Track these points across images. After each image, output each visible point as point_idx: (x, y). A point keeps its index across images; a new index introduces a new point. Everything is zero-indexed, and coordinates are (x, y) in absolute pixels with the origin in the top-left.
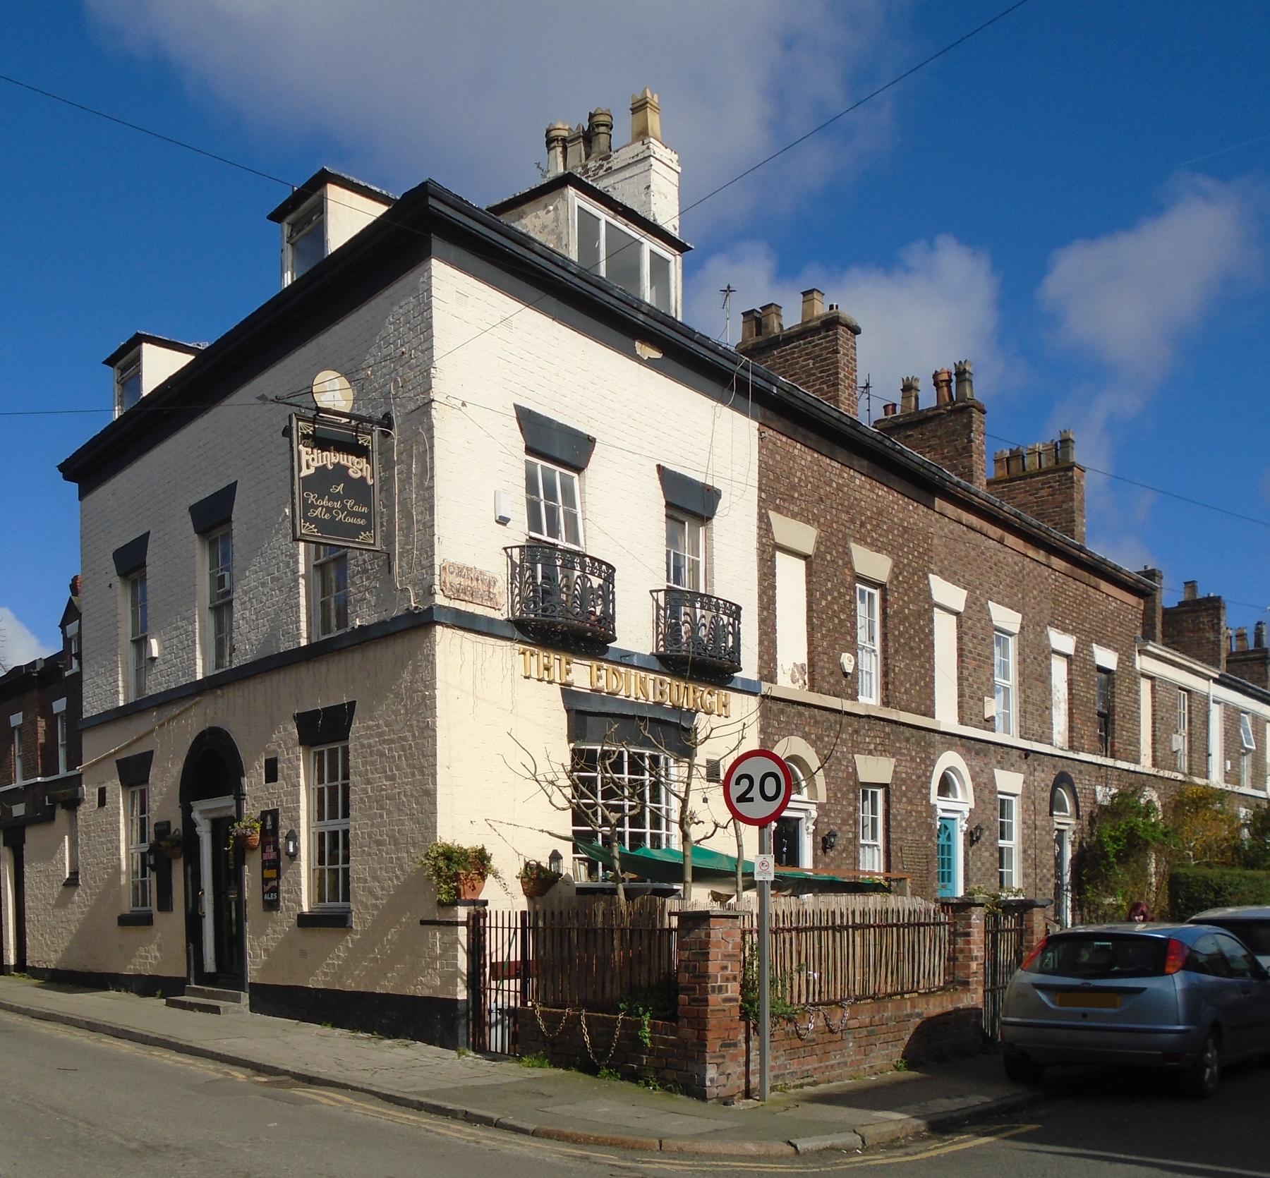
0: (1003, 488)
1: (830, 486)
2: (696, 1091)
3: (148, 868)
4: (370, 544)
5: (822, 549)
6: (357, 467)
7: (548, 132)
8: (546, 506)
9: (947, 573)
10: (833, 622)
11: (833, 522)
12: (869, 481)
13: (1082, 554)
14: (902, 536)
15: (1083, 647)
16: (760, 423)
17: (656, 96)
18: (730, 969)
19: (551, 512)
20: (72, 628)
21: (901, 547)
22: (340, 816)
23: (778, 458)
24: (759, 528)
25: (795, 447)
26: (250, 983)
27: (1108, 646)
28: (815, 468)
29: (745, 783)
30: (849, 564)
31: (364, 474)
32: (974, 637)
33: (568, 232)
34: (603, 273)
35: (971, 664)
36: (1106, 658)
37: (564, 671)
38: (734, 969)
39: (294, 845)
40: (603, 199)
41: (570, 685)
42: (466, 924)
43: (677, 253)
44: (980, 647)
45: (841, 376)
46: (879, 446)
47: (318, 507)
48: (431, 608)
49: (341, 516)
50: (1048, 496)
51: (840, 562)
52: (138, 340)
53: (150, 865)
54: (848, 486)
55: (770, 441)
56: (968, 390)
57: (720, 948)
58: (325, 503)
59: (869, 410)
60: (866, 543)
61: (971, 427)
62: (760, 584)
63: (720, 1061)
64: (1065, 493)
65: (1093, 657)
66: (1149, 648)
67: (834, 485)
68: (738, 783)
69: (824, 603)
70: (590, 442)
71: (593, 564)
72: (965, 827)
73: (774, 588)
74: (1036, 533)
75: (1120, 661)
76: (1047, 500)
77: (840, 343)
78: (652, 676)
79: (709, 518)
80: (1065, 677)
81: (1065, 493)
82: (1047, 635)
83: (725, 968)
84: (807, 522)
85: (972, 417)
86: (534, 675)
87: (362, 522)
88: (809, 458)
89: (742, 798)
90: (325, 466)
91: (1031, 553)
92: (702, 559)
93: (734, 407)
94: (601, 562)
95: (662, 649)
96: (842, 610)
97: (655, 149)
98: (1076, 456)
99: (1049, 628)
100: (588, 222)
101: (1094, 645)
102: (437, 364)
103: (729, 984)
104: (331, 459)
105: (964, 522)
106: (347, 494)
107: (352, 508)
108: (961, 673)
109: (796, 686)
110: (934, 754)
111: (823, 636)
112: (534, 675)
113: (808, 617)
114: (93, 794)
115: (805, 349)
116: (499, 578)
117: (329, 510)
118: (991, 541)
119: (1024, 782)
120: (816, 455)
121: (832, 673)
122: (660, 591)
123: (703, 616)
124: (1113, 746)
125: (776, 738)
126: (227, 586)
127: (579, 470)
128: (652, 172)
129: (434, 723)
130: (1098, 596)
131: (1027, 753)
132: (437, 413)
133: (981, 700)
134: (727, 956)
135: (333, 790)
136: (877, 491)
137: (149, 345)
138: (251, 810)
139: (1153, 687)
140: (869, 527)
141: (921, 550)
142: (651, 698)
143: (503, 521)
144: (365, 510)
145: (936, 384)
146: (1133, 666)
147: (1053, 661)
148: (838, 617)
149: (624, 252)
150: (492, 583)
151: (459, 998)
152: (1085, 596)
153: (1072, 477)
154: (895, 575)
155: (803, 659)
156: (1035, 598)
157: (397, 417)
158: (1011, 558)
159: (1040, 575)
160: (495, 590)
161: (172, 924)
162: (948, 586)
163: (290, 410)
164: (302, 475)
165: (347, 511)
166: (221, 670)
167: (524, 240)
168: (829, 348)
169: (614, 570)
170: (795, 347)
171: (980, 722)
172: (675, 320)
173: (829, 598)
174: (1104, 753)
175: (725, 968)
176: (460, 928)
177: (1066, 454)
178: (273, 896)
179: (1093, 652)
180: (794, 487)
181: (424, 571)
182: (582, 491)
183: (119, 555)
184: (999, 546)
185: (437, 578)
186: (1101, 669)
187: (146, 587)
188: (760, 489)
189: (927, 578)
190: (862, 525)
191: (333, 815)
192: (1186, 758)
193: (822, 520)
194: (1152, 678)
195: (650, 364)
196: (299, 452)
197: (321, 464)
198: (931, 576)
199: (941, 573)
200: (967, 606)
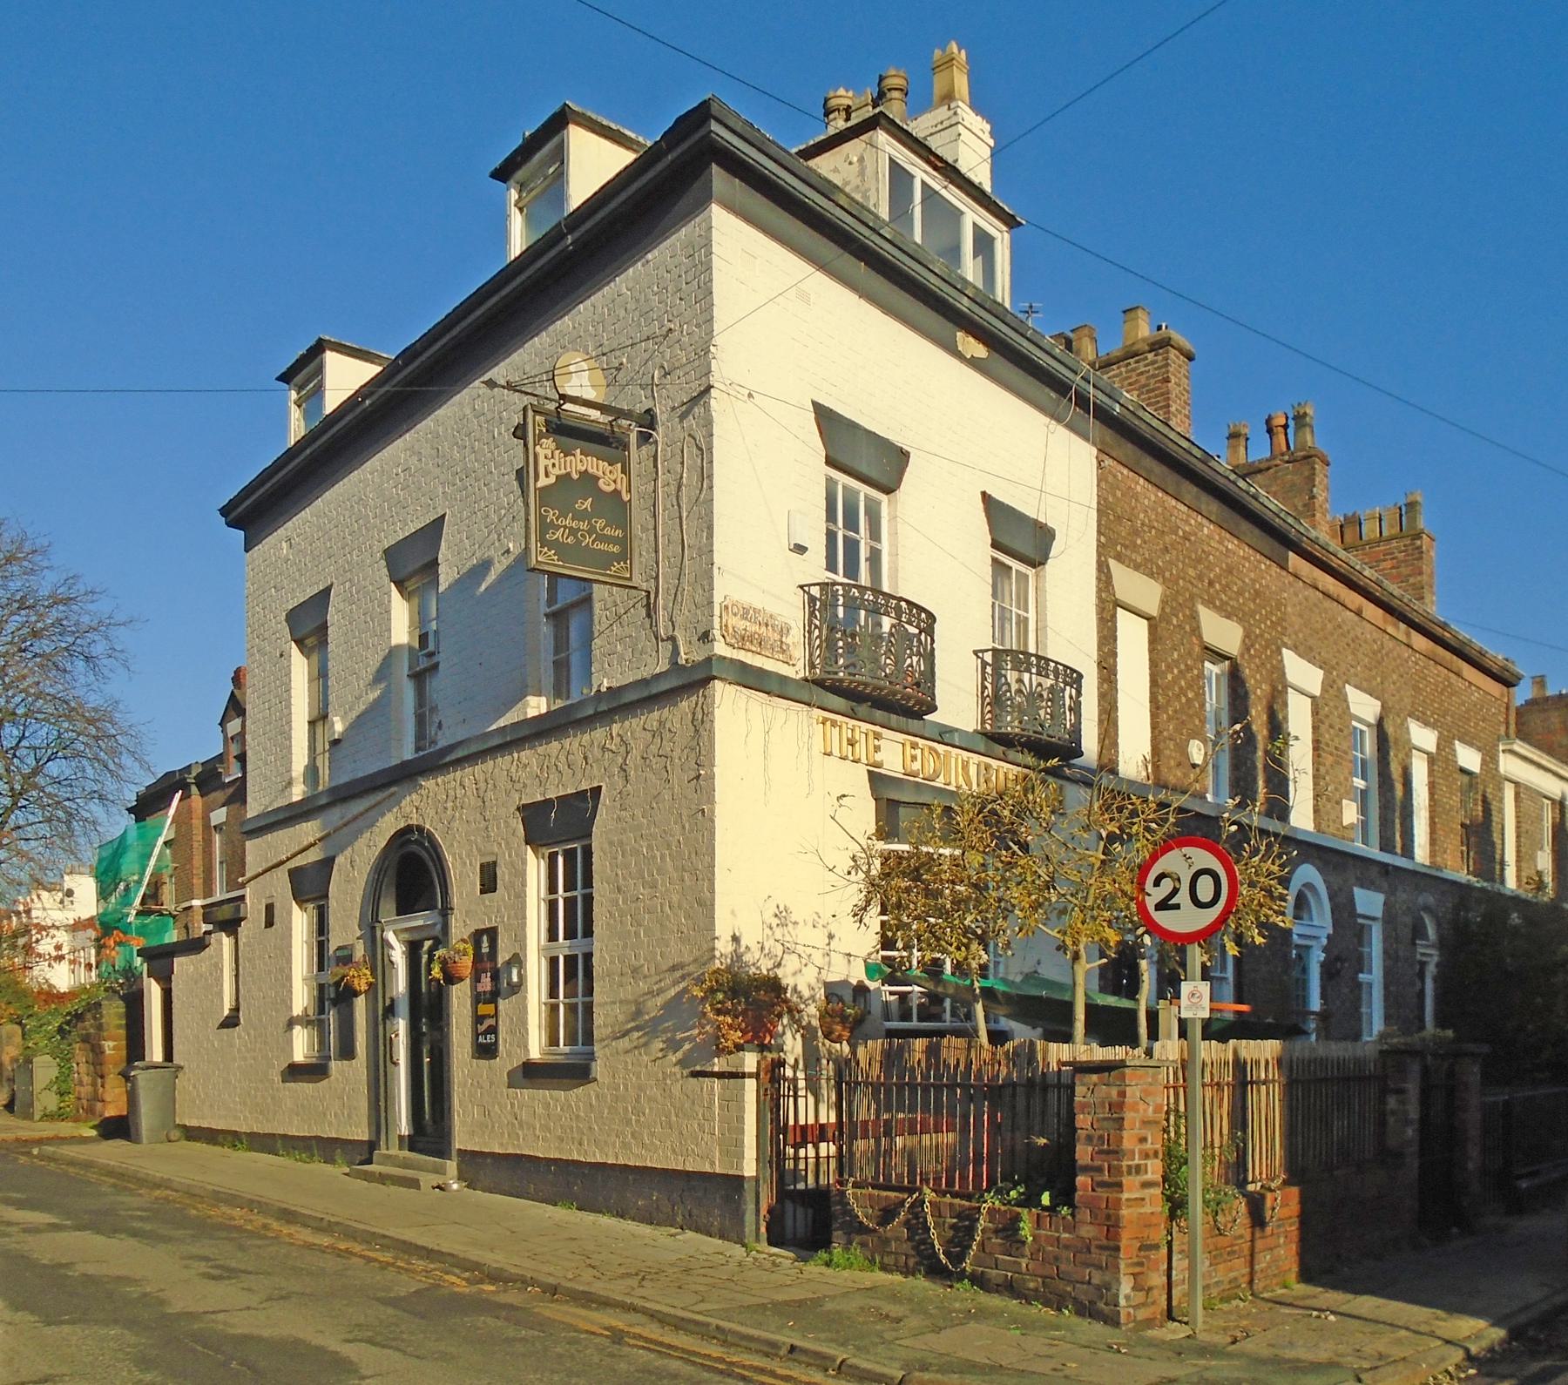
1: (1176, 535)
2: (1099, 1309)
3: (327, 1003)
4: (626, 579)
5: (1168, 610)
6: (609, 477)
7: (826, 100)
8: (844, 536)
9: (1301, 648)
10: (1180, 701)
11: (1179, 578)
12: (1218, 530)
14: (1254, 601)
15: (1445, 743)
16: (1099, 450)
17: (963, 52)
18: (1150, 1140)
19: (852, 547)
20: (234, 726)
21: (1252, 614)
23: (1119, 494)
24: (1098, 579)
25: (1137, 483)
26: (459, 1150)
27: (1470, 744)
28: (1160, 510)
29: (1167, 885)
30: (1196, 630)
31: (619, 487)
32: (1331, 726)
33: (877, 190)
34: (918, 238)
35: (1329, 760)
36: (1469, 758)
37: (871, 748)
38: (1155, 1143)
39: (519, 973)
40: (919, 147)
41: (879, 766)
42: (757, 1076)
43: (1005, 228)
44: (1336, 740)
45: (1173, 409)
46: (1231, 486)
47: (558, 527)
48: (709, 660)
49: (588, 540)
51: (1187, 628)
52: (319, 348)
53: (329, 999)
54: (1196, 534)
55: (1110, 472)
56: (1309, 437)
57: (1137, 1111)
58: (568, 522)
60: (1215, 606)
61: (1314, 480)
62: (1099, 649)
63: (1137, 1270)
64: (1413, 565)
65: (1455, 756)
67: (1181, 533)
68: (1157, 883)
69: (1170, 677)
70: (902, 456)
71: (911, 611)
72: (1322, 956)
73: (1115, 655)
75: (1484, 763)
77: (1171, 369)
78: (976, 758)
79: (1043, 563)
80: (1426, 780)
81: (1413, 565)
82: (1408, 728)
83: (1143, 1140)
84: (1151, 575)
85: (1314, 469)
86: (836, 752)
87: (616, 549)
88: (1153, 498)
89: (1163, 906)
90: (568, 474)
92: (1032, 616)
93: (1070, 427)
94: (921, 609)
95: (988, 727)
96: (1190, 687)
97: (965, 116)
99: (1409, 719)
100: (899, 176)
101: (1457, 742)
102: (717, 340)
103: (1149, 1162)
104: (581, 462)
106: (596, 512)
107: (602, 530)
108: (1318, 770)
111: (1170, 719)
112: (836, 752)
113: (1151, 693)
114: (259, 911)
115: (1127, 378)
116: (793, 624)
117: (573, 532)
118: (1348, 613)
119: (1385, 904)
120: (1160, 494)
121: (1179, 764)
122: (987, 651)
123: (1040, 685)
126: (431, 647)
127: (888, 490)
128: (961, 145)
129: (712, 811)
130: (1460, 684)
132: (718, 402)
133: (1339, 803)
134: (1146, 1123)
135: (570, 903)
136: (1226, 543)
137: (334, 354)
138: (460, 929)
139: (1517, 795)
140: (1217, 586)
141: (1274, 619)
142: (975, 787)
143: (800, 549)
144: (619, 533)
145: (1270, 431)
146: (1497, 769)
148: (1186, 696)
149: (941, 215)
150: (784, 631)
151: (746, 1174)
153: (1421, 547)
154: (1247, 646)
155: (1147, 749)
156: (1394, 683)
157: (662, 412)
158: (1369, 633)
159: (1399, 656)
160: (788, 640)
161: (351, 1075)
162: (1304, 664)
163: (527, 400)
164: (539, 485)
165: (598, 534)
166: (421, 753)
167: (827, 189)
168: (1157, 375)
169: (934, 619)
170: (1114, 376)
172: (1001, 305)
173: (1176, 671)
175: (1143, 1140)
176: (747, 1081)
177: (1413, 520)
178: (490, 1038)
179: (1455, 750)
180: (1136, 533)
181: (699, 612)
182: (893, 518)
183: (293, 617)
184: (1356, 618)
185: (716, 620)
186: (1463, 771)
187: (327, 653)
188: (1099, 533)
189: (1280, 653)
190: (1211, 584)
191: (570, 934)
192: (402, 1025)
193: (1167, 574)
194: (1517, 784)
195: (974, 363)
196: (536, 456)
197: (563, 472)
198: (1284, 651)
199: (1295, 649)
200: (1324, 690)
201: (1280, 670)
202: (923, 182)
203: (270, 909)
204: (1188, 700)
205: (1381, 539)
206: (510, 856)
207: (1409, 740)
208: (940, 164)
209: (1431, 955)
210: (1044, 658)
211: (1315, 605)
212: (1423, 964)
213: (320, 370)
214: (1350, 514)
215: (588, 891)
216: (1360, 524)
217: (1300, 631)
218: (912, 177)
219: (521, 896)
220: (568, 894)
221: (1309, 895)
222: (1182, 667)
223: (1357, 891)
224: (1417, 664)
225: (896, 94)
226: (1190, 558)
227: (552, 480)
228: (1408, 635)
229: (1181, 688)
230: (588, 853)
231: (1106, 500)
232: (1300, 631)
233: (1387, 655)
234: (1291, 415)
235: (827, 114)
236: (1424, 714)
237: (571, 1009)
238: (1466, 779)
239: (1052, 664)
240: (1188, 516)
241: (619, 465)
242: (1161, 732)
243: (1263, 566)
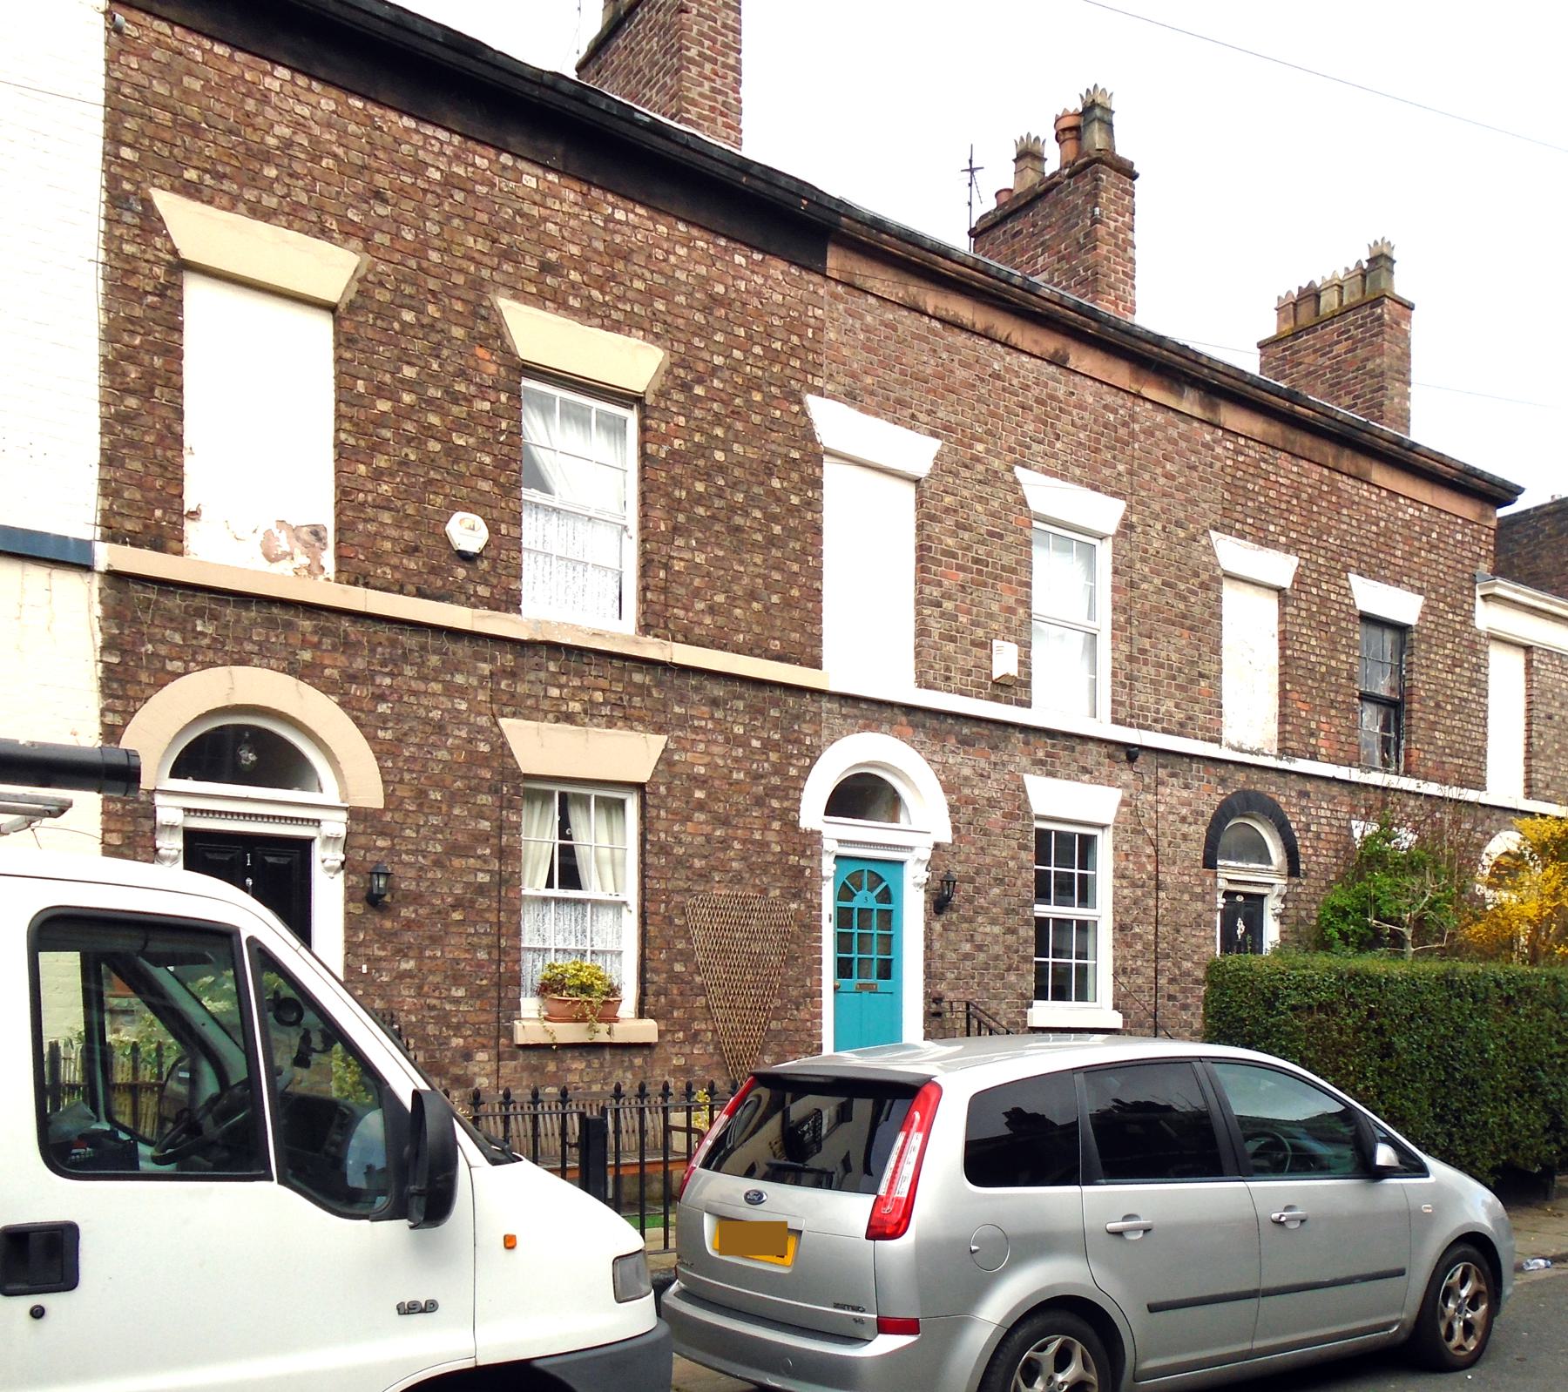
0: (1284, 350)
13: (1298, 408)
22: (856, 911)
50: (1346, 353)
59: (970, 204)
66: (1498, 591)
74: (1151, 352)
76: (1345, 361)
81: (1371, 344)
91: (1151, 392)
98: (1402, 285)
105: (930, 311)
109: (285, 568)
110: (817, 734)
124: (1408, 756)
125: (176, 666)
131: (1131, 753)
147: (534, 428)
152: (1325, 488)
171: (980, 686)
174: (1393, 768)
201: (805, 434)
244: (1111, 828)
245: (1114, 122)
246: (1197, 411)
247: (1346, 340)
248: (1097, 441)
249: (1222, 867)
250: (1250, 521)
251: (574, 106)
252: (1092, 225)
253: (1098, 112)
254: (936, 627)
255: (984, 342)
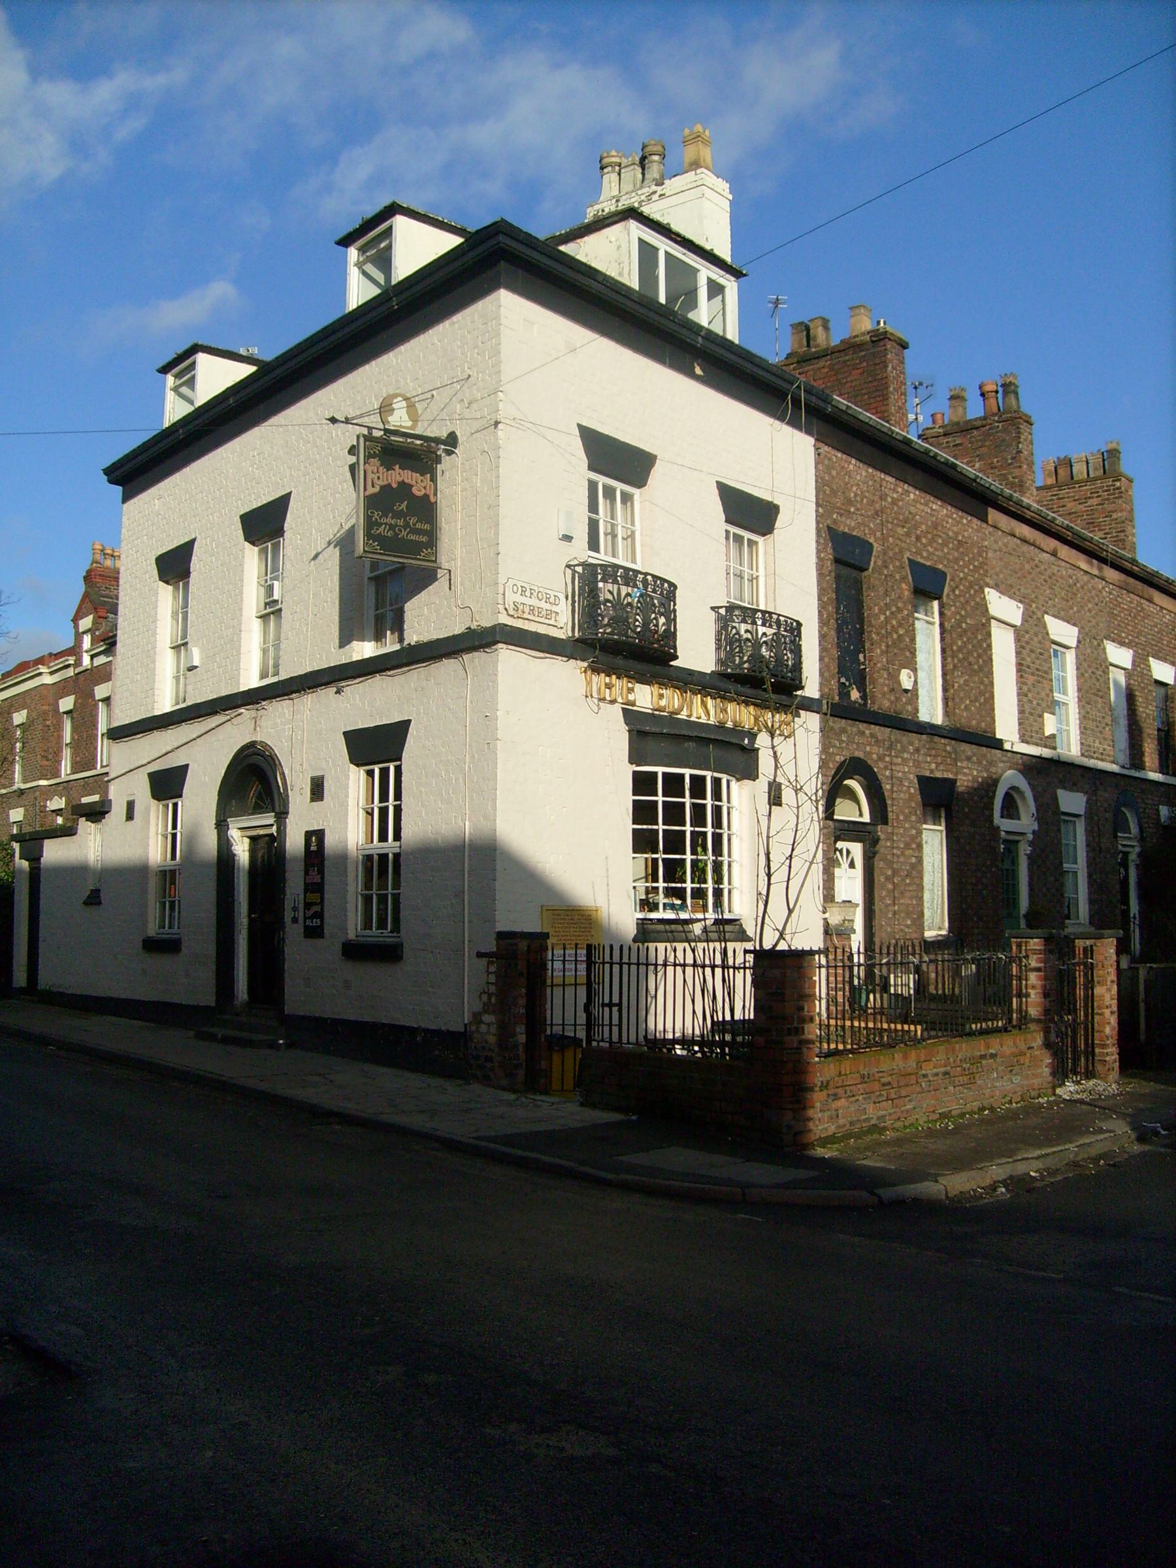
4: (433, 561)
9: (1002, 587)
15: (1140, 661)
23: (834, 473)
27: (1165, 660)
32: (1032, 651)
41: (633, 704)
44: (1038, 662)
47: (380, 525)
50: (1097, 505)
54: (903, 500)
58: (389, 520)
65: (1150, 671)
72: (1029, 850)
76: (1097, 510)
81: (1114, 503)
82: (1104, 649)
88: (864, 474)
98: (1126, 466)
105: (1017, 535)
117: (392, 527)
122: (721, 607)
130: (1152, 609)
133: (1041, 716)
137: (205, 355)
141: (976, 563)
156: (1090, 611)
164: (368, 493)
169: (675, 587)
173: (888, 613)
179: (1149, 666)
180: (850, 502)
184: (1053, 558)
189: (983, 592)
190: (918, 538)
199: (996, 587)
200: (1024, 620)
201: (983, 607)
202: (666, 252)
203: (131, 806)
204: (900, 636)
205: (1089, 479)
206: (335, 771)
207: (1106, 659)
208: (679, 239)
209: (1133, 846)
210: (766, 612)
211: (1014, 550)
212: (1126, 854)
213: (193, 366)
214: (1062, 457)
215: (398, 802)
216: (1071, 466)
217: (1001, 571)
218: (657, 249)
219: (344, 805)
220: (386, 804)
221: (1015, 796)
222: (894, 609)
223: (1060, 793)
224: (1110, 593)
225: (656, 158)
226: (898, 519)
227: (377, 489)
228: (1100, 569)
229: (893, 627)
230: (398, 770)
231: (822, 478)
232: (1001, 571)
233: (1082, 587)
234: (1000, 384)
235: (602, 168)
236: (1120, 636)
237: (383, 899)
238: (1162, 690)
239: (775, 617)
240: (896, 485)
241: (428, 475)
242: (875, 664)
243: (965, 521)
244: (1083, 817)
245: (1019, 392)
246: (1095, 572)
247: (1097, 497)
248: (1067, 595)
249: (1120, 837)
250: (1116, 632)
251: (903, 447)
252: (1016, 454)
253: (1013, 387)
254: (1027, 709)
255: (1033, 547)
